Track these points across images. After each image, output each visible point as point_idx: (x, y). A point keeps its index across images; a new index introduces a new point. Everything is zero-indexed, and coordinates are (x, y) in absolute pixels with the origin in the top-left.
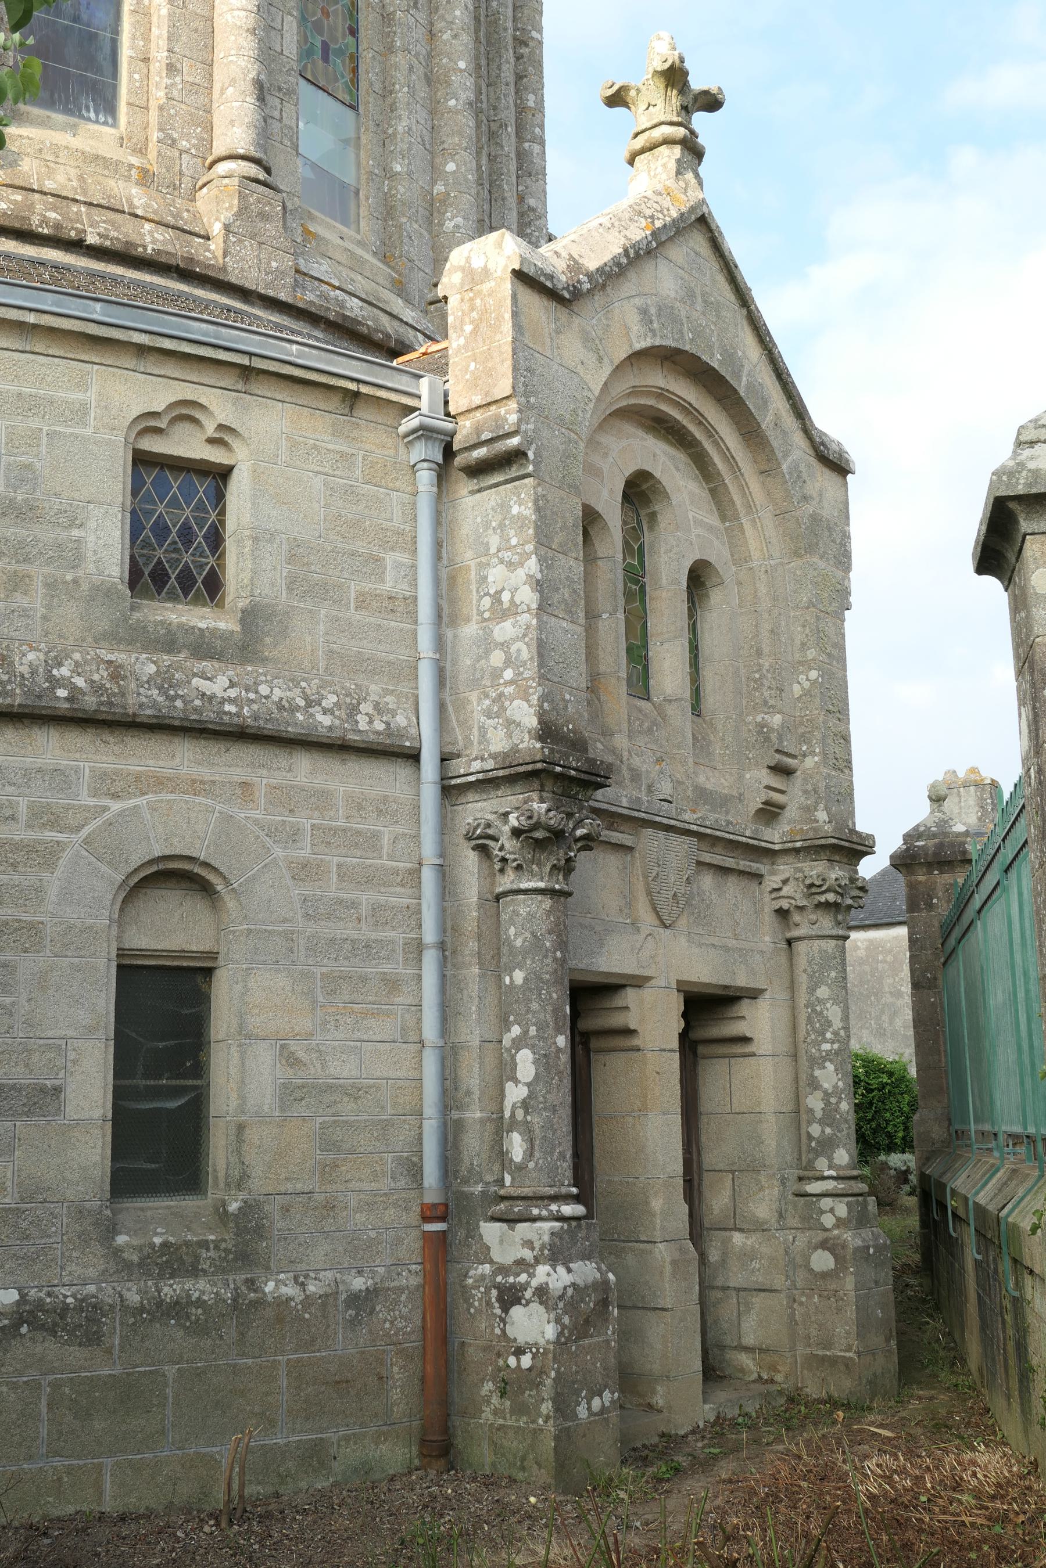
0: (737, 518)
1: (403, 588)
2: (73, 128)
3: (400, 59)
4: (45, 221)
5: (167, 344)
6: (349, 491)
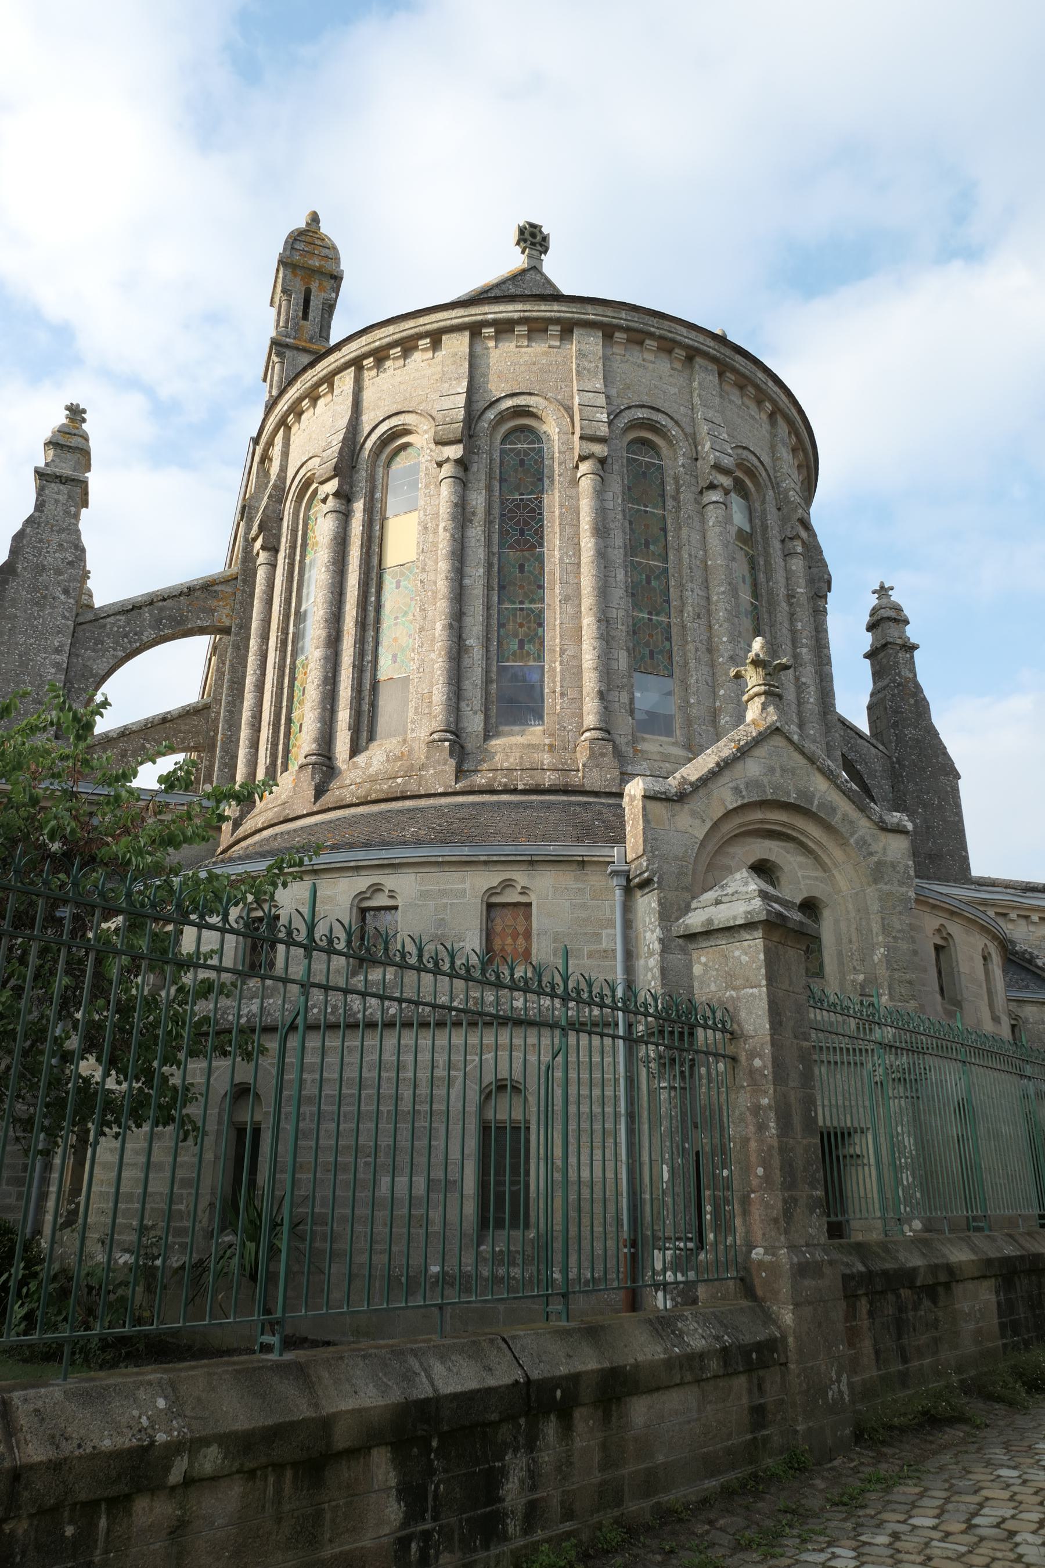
0: (830, 871)
1: (611, 946)
2: (522, 733)
3: (691, 647)
4: (500, 784)
5: (495, 858)
6: (584, 905)
